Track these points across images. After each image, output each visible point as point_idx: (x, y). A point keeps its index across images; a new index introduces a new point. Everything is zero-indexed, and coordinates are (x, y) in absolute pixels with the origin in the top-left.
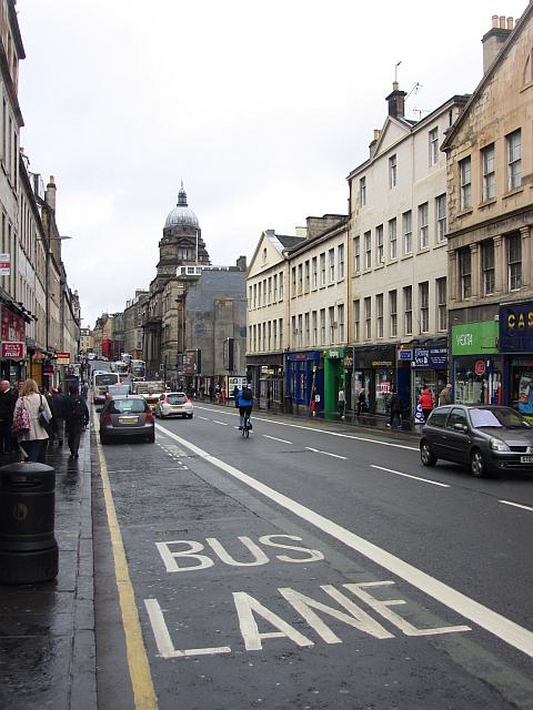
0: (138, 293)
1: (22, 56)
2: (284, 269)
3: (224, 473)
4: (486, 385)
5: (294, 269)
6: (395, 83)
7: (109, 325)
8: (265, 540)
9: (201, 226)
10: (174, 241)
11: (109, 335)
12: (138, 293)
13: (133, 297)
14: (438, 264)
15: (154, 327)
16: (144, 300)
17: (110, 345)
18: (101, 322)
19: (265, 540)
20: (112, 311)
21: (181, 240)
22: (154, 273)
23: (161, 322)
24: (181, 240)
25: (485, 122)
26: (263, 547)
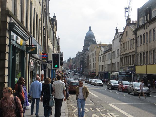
0: (79, 52)
1: (57, 31)
2: (104, 55)
3: (30, 76)
4: (26, 89)
5: (121, 44)
6: (117, 28)
7: (71, 61)
8: (99, 108)
9: (95, 36)
10: (88, 40)
11: (71, 64)
12: (79, 52)
13: (77, 53)
14: (118, 60)
15: (82, 63)
16: (80, 55)
17: (71, 66)
18: (69, 60)
19: (99, 108)
20: (72, 57)
21: (90, 39)
22: (82, 48)
23: (84, 61)
24: (90, 39)
25: (123, 40)
26: (99, 109)
